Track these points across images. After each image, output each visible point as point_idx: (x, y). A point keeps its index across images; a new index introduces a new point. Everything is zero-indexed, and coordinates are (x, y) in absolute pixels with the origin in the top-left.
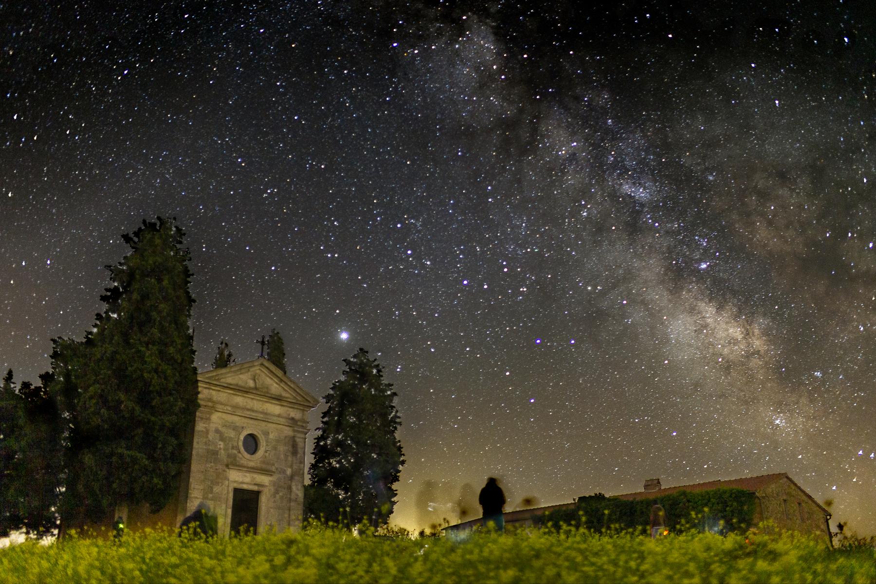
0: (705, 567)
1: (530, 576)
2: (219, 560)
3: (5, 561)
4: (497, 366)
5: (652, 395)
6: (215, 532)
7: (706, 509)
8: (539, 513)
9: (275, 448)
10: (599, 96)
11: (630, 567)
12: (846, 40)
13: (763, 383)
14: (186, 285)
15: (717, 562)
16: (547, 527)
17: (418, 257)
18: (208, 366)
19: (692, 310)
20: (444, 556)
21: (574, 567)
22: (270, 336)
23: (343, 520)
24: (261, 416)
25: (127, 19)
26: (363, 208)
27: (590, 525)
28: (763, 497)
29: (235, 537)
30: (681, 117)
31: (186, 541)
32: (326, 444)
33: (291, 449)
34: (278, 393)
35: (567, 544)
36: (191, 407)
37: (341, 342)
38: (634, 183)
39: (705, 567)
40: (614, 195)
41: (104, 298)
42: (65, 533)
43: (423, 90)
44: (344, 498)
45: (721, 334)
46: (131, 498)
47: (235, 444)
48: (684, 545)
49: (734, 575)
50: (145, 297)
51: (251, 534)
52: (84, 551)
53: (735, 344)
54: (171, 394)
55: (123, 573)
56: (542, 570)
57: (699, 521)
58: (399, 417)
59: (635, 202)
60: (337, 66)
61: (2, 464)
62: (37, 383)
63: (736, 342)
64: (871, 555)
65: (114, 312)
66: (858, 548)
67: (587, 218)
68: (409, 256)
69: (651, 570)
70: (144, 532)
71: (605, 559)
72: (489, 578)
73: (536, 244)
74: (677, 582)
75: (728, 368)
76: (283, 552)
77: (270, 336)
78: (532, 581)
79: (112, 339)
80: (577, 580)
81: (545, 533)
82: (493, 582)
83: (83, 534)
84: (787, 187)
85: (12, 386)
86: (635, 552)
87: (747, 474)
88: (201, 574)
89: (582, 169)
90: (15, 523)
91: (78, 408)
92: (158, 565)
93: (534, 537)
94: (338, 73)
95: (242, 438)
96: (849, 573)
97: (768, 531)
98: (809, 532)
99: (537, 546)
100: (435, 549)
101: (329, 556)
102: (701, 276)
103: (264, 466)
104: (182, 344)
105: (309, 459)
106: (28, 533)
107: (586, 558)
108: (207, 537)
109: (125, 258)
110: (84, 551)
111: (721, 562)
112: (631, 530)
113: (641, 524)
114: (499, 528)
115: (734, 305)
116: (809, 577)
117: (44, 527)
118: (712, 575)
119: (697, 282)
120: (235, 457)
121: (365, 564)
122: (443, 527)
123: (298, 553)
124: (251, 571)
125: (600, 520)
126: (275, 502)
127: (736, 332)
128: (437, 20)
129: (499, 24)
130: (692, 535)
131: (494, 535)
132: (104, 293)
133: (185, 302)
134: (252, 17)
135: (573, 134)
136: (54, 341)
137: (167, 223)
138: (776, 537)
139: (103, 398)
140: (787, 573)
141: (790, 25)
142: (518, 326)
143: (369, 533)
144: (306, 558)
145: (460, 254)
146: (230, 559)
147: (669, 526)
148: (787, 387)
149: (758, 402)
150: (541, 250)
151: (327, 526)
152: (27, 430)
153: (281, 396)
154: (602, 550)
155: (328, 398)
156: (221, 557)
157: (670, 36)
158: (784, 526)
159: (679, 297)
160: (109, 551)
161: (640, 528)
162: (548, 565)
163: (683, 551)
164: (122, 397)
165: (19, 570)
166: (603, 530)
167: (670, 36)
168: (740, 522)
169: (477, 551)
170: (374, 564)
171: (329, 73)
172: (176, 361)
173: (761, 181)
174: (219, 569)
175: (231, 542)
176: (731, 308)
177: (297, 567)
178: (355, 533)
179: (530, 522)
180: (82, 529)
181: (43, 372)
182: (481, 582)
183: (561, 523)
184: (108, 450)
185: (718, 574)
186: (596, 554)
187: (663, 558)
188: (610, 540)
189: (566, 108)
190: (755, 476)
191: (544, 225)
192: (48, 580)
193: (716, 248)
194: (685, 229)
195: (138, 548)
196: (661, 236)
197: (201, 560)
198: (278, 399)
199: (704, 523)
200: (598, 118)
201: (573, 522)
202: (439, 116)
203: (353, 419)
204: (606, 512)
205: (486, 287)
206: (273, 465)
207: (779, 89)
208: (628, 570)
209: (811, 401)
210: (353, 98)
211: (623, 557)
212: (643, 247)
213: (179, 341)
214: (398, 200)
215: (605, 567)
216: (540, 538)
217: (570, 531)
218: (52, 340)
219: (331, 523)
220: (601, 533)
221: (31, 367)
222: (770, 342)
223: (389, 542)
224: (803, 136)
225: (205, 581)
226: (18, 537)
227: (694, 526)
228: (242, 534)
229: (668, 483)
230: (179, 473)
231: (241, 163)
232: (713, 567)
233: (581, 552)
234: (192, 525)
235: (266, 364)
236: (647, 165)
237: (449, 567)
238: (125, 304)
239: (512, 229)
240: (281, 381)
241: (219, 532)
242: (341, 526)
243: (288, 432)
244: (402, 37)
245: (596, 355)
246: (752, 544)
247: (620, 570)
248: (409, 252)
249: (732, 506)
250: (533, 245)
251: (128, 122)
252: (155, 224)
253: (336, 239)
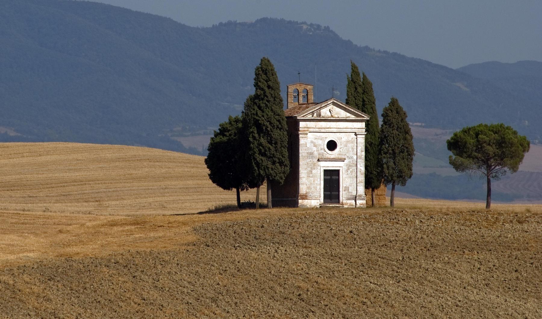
47: (322, 147)
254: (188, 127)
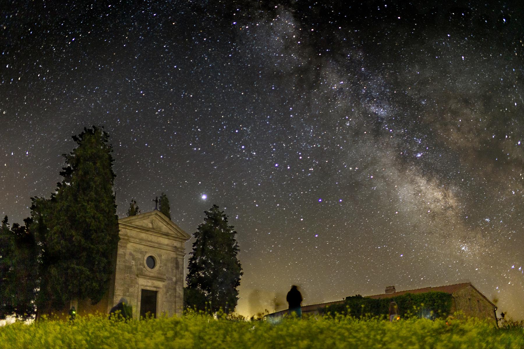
0: (422, 339)
1: (317, 344)
2: (134, 334)
3: (3, 335)
4: (296, 215)
5: (388, 233)
6: (131, 316)
7: (422, 304)
8: (323, 307)
9: (166, 265)
10: (356, 54)
11: (377, 339)
12: (504, 20)
13: (454, 225)
14: (110, 166)
15: (429, 336)
16: (327, 315)
17: (248, 150)
18: (125, 215)
19: (412, 182)
20: (266, 332)
21: (343, 339)
22: (161, 197)
23: (207, 309)
24: (156, 245)
25: (74, 8)
26: (215, 121)
27: (353, 314)
28: (457, 297)
29: (143, 319)
30: (405, 66)
31: (113, 322)
32: (195, 262)
33: (175, 265)
34: (166, 231)
35: (339, 325)
36: (115, 239)
37: (202, 201)
38: (378, 106)
39: (422, 339)
40: (365, 113)
41: (62, 174)
42: (40, 317)
43: (251, 50)
44: (208, 296)
45: (429, 196)
46: (80, 295)
47: (142, 262)
48: (409, 326)
49: (439, 344)
50: (86, 173)
51: (153, 318)
52: (51, 328)
53: (438, 202)
54: (103, 232)
55: (75, 342)
56: (324, 341)
57: (418, 312)
58: (238, 246)
59: (378, 117)
60: (200, 36)
61: (1, 274)
62: (22, 224)
63: (438, 201)
64: (521, 332)
65: (68, 182)
66: (513, 327)
67: (349, 126)
68: (243, 149)
69: (390, 341)
70: (88, 316)
71: (362, 334)
72: (293, 345)
73: (319, 142)
74: (405, 348)
75: (433, 216)
76: (172, 329)
77: (161, 197)
78: (318, 347)
79: (67, 198)
80: (345, 347)
81: (326, 319)
82: (295, 348)
83: (51, 318)
84: (469, 108)
85: (7, 226)
86: (380, 330)
87: (447, 283)
88: (123, 343)
89: (346, 97)
90: (9, 311)
91: (47, 240)
92: (97, 337)
93: (319, 321)
94: (200, 40)
95: (146, 258)
96: (508, 342)
97: (460, 317)
98: (484, 318)
99: (322, 326)
100: (260, 328)
101: (200, 332)
102: (418, 162)
103: (159, 276)
104: (109, 201)
105: (186, 272)
106: (17, 317)
107: (350, 333)
108: (126, 320)
109: (74, 150)
110: (51, 328)
111: (431, 336)
112: (377, 317)
113: (384, 313)
114: (299, 316)
115: (437, 179)
116: (484, 345)
117: (27, 313)
118: (426, 344)
119: (415, 165)
120: (142, 270)
121: (222, 336)
122: (265, 315)
123: (181, 329)
124: (153, 341)
125: (359, 311)
126: (166, 298)
127: (438, 195)
128: (259, 9)
129: (297, 11)
130: (414, 320)
131: (295, 320)
132: (62, 171)
133: (110, 177)
134: (149, 7)
135: (341, 76)
136: (32, 199)
137: (98, 129)
138: (464, 321)
139: (62, 233)
140: (471, 342)
141: (471, 11)
142: (308, 191)
143: (223, 317)
144: (186, 333)
145: (273, 148)
146: (140, 333)
147: (400, 314)
148: (469, 228)
149: (452, 237)
150: (322, 146)
151: (198, 313)
152: (17, 253)
153: (168, 233)
154: (360, 328)
155: (196, 234)
156: (135, 332)
157: (399, 18)
158: (469, 315)
159: (404, 174)
160: (67, 328)
161: (383, 315)
162: (328, 338)
163: (408, 329)
164: (74, 233)
165: (12, 340)
166: (361, 317)
167: (399, 18)
168: (442, 312)
169: (285, 329)
170: (227, 337)
171: (195, 40)
172: (105, 211)
173: (453, 105)
174: (134, 340)
175: (141, 323)
176: (435, 181)
177: (181, 338)
178: (215, 317)
179: (317, 312)
180: (50, 314)
181: (26, 218)
182: (288, 348)
183: (336, 313)
184: (65, 265)
185: (430, 343)
186: (357, 331)
187: (397, 334)
188: (365, 323)
189: (337, 61)
190: (452, 284)
191: (324, 131)
192: (30, 347)
193: (426, 145)
194: (408, 133)
195: (84, 327)
196: (393, 138)
197: (123, 334)
198: (167, 235)
199: (421, 312)
200: (356, 67)
201: (343, 312)
202: (261, 66)
203: (211, 248)
204: (363, 306)
205: (289, 168)
206: (165, 275)
207: (464, 49)
208: (376, 341)
209: (483, 236)
210: (209, 55)
211: (373, 333)
212: (383, 144)
213: (107, 200)
214: (237, 116)
215: (362, 339)
216: (323, 321)
217: (341, 317)
218: (31, 198)
219: (200, 311)
220: (359, 318)
221: (19, 215)
222: (459, 201)
223: (235, 323)
224: (478, 77)
225: (126, 347)
226: (11, 319)
227: (415, 314)
228: (147, 318)
229: (400, 289)
230: (108, 280)
231: (142, 93)
232: (426, 339)
233: (348, 330)
234: (117, 312)
235: (159, 214)
236: (386, 95)
237: (269, 339)
238: (74, 177)
239: (305, 133)
240: (168, 224)
241: (133, 317)
242: (206, 313)
243: (173, 255)
244: (239, 18)
245: (355, 208)
246: (450, 325)
247: (371, 341)
248: (243, 147)
249: (438, 302)
250: (317, 143)
251: (75, 69)
252: (91, 130)
253: (199, 139)
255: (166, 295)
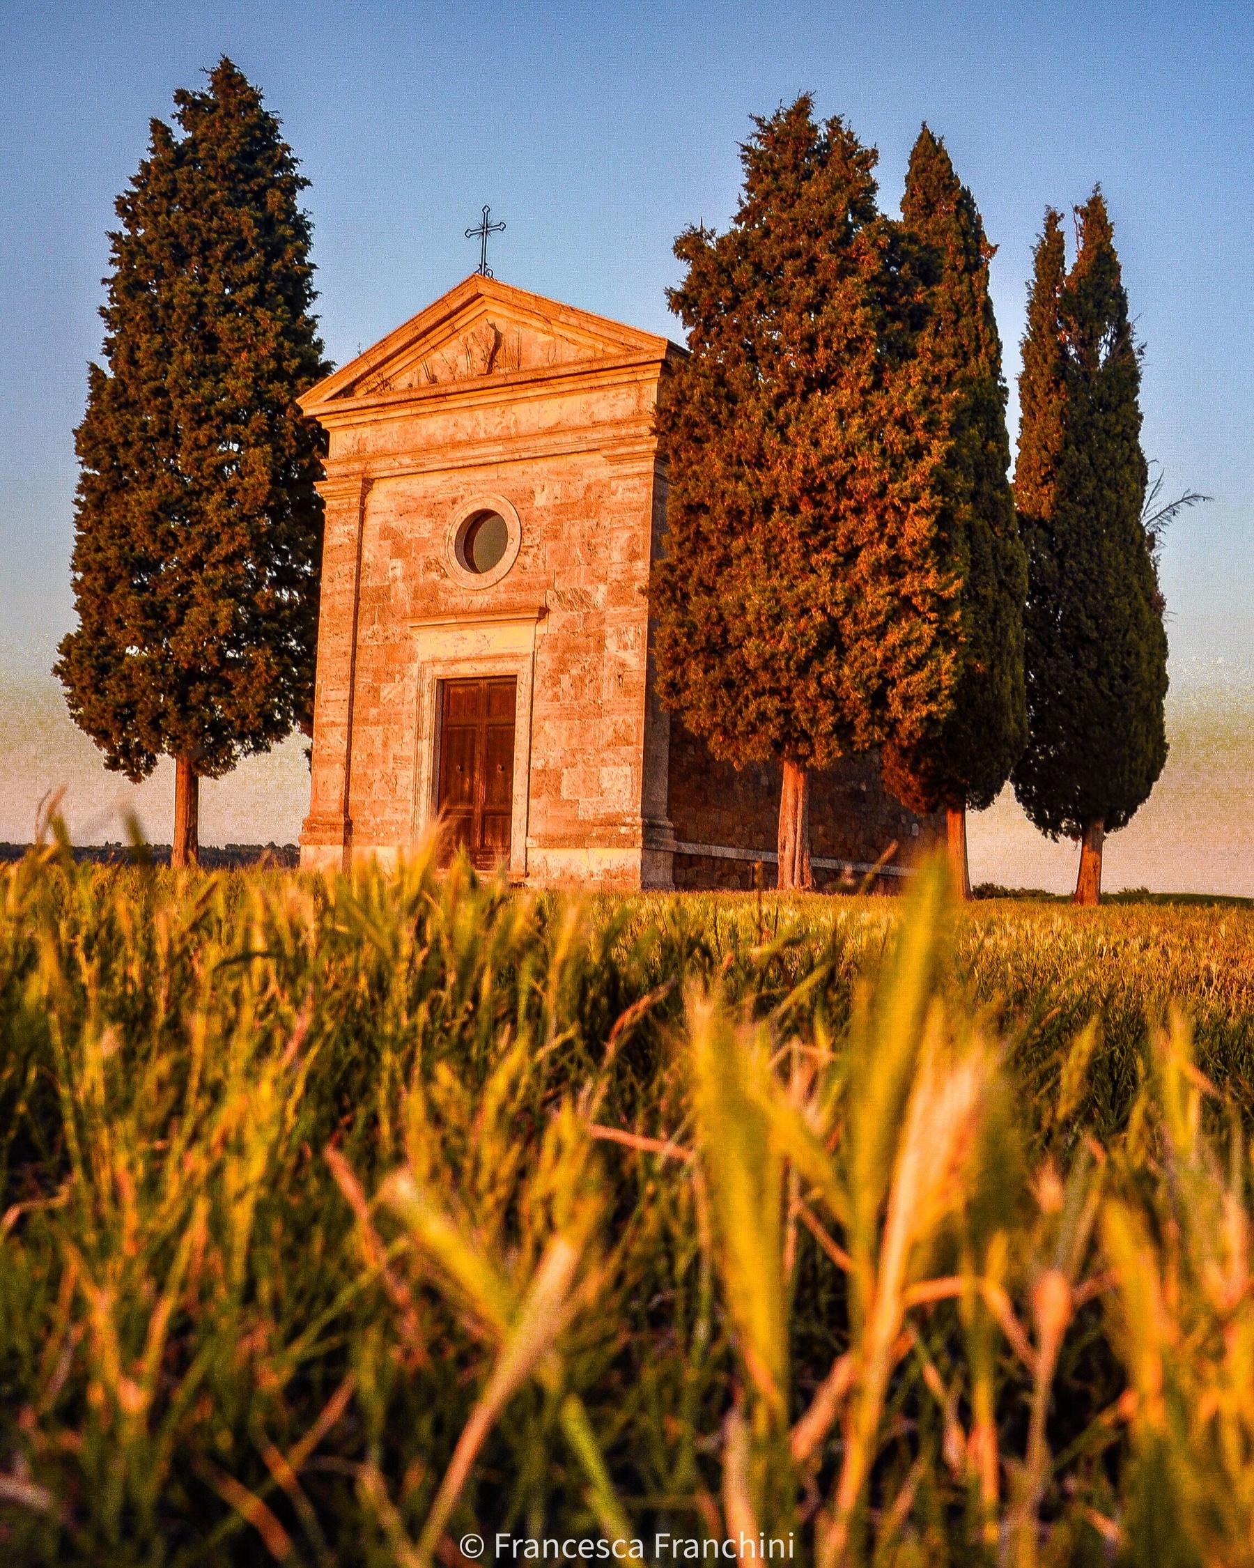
24: (495, 452)
254: (1220, 661)
255: (556, 683)
